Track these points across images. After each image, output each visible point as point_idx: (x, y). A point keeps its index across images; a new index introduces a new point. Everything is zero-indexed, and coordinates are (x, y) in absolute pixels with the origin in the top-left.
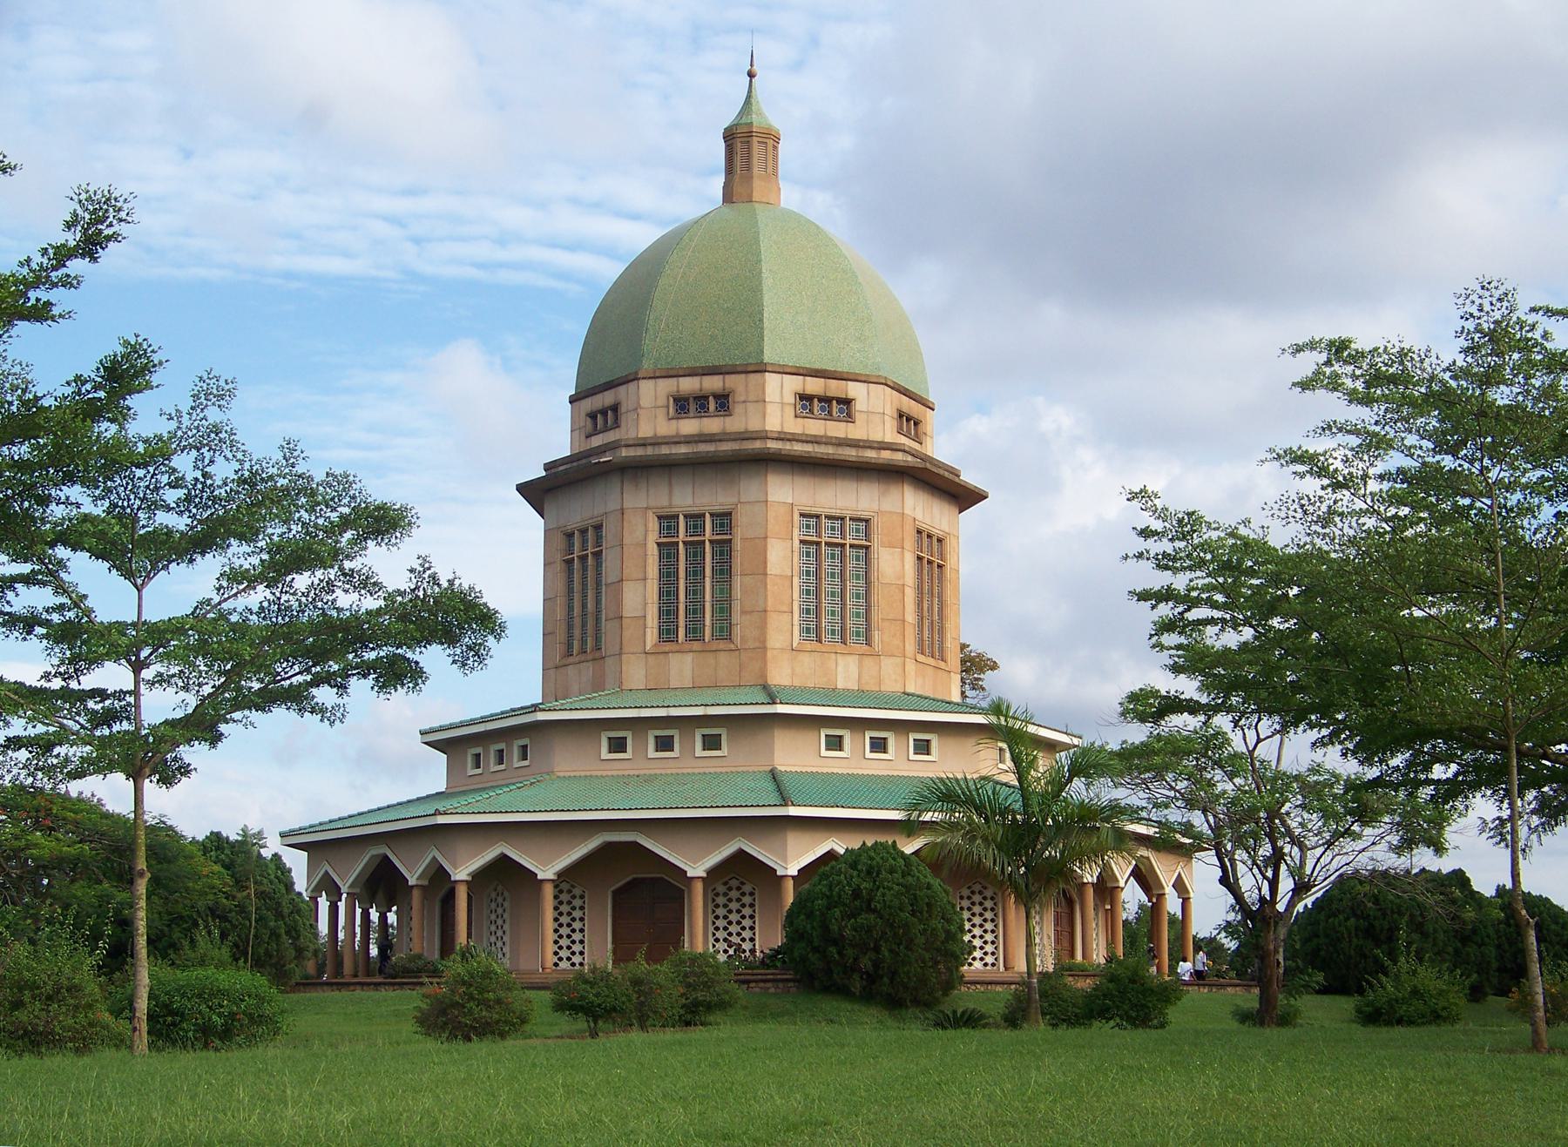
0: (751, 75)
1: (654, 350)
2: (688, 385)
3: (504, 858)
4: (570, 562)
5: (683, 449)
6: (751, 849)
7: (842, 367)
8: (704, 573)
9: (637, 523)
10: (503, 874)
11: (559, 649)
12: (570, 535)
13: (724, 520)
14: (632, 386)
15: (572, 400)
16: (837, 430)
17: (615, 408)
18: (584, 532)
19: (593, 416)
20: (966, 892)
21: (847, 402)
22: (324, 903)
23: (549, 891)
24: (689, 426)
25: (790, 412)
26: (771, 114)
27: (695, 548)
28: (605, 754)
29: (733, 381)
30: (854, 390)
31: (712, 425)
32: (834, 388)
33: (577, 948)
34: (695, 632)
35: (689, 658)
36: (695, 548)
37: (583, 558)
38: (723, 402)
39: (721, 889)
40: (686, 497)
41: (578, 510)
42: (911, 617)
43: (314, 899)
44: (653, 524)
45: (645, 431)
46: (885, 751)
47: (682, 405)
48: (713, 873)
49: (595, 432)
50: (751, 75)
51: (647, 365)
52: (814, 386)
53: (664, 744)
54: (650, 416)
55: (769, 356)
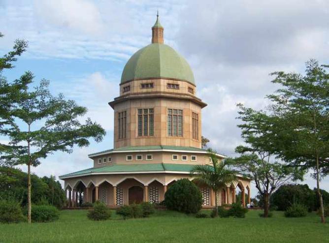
0: (158, 16)
1: (137, 74)
2: (145, 82)
3: (155, 181)
4: (119, 119)
5: (143, 95)
6: (158, 180)
7: (177, 78)
8: (148, 121)
9: (134, 111)
10: (106, 185)
11: (117, 138)
12: (120, 113)
13: (152, 110)
14: (132, 82)
15: (120, 85)
16: (176, 91)
17: (129, 86)
18: (122, 113)
19: (124, 88)
20: (203, 189)
21: (178, 85)
22: (68, 191)
23: (115, 189)
24: (145, 90)
25: (166, 88)
26: (162, 24)
27: (146, 116)
28: (127, 160)
29: (153, 81)
30: (179, 83)
31: (150, 90)
32: (175, 82)
33: (121, 198)
34: (146, 134)
35: (144, 139)
36: (146, 116)
37: (122, 118)
38: (152, 85)
39: (151, 188)
40: (144, 105)
41: (121, 108)
42: (191, 131)
43: (66, 191)
44: (137, 111)
45: (135, 91)
46: (195, 159)
47: (143, 86)
48: (119, 186)
49: (125, 91)
50: (158, 16)
51: (136, 77)
52: (171, 82)
53: (185, 158)
54: (136, 88)
55: (162, 75)
